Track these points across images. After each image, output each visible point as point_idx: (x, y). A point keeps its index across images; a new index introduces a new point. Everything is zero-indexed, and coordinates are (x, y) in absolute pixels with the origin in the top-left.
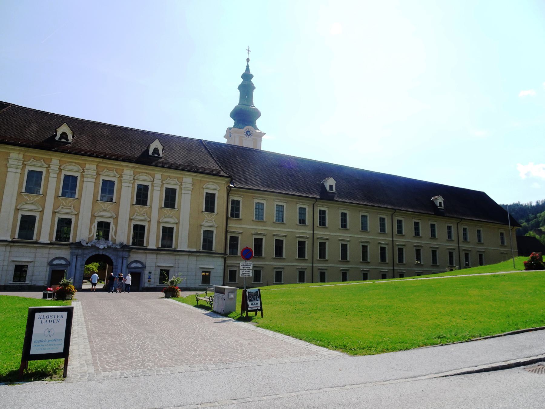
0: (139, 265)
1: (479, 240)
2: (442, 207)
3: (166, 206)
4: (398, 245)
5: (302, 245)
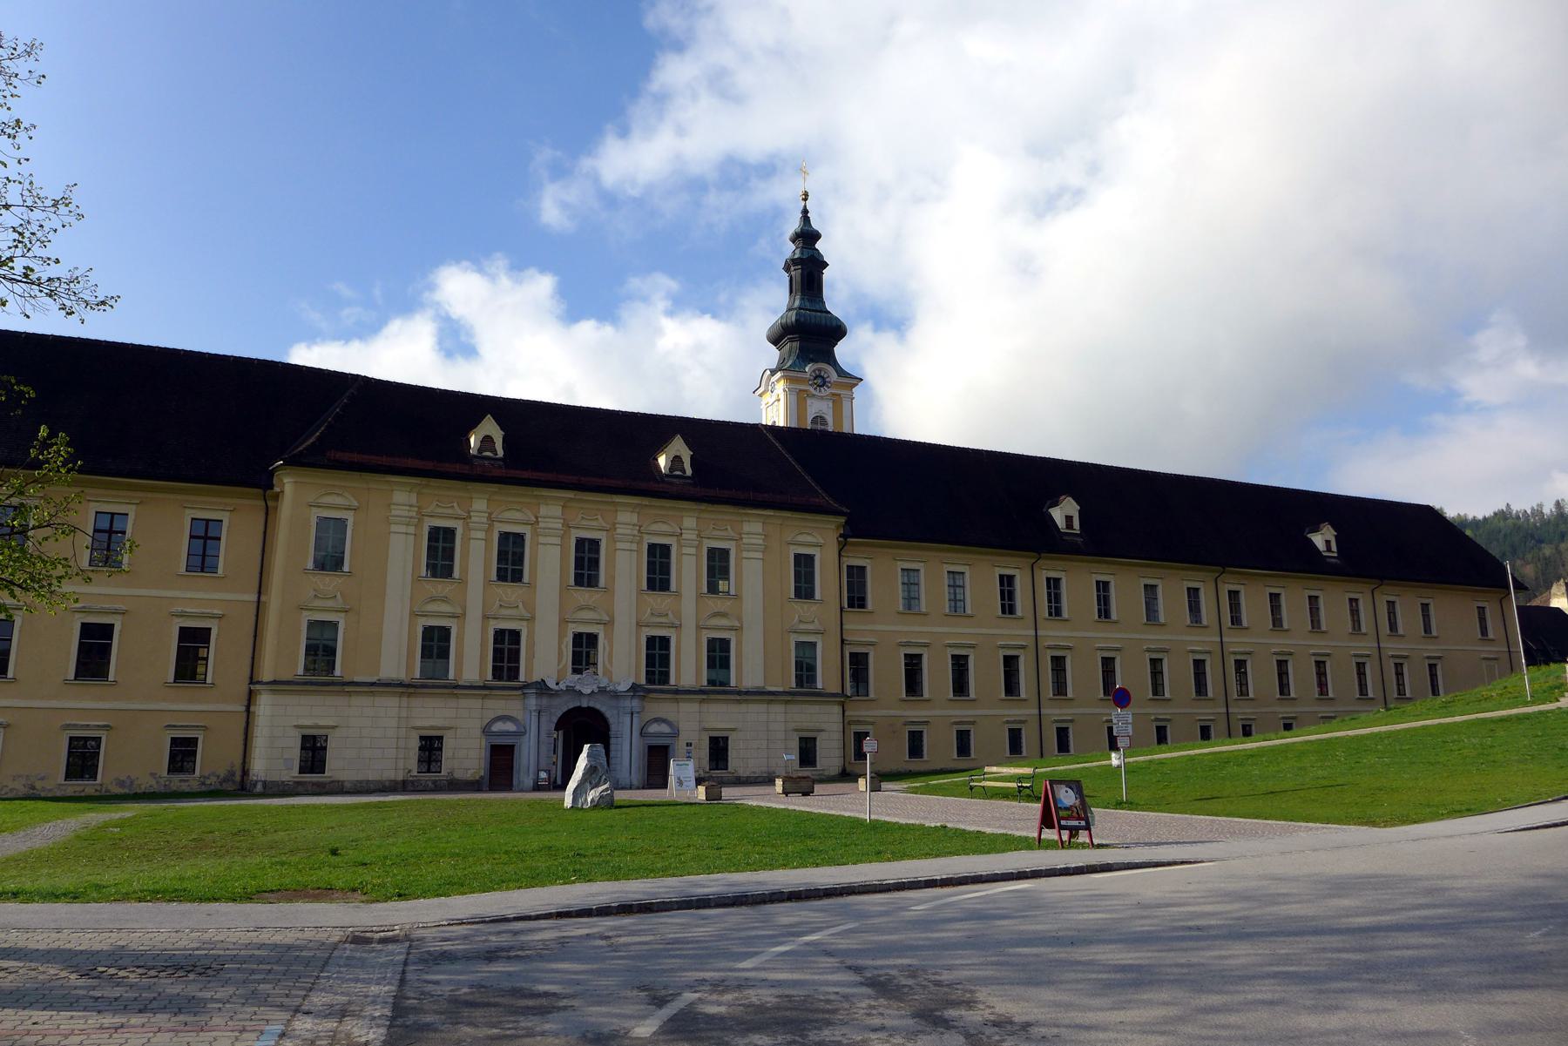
0: (665, 728)
1: (1427, 629)
2: (1333, 552)
3: (502, 576)
4: (1235, 653)
5: (1010, 663)
